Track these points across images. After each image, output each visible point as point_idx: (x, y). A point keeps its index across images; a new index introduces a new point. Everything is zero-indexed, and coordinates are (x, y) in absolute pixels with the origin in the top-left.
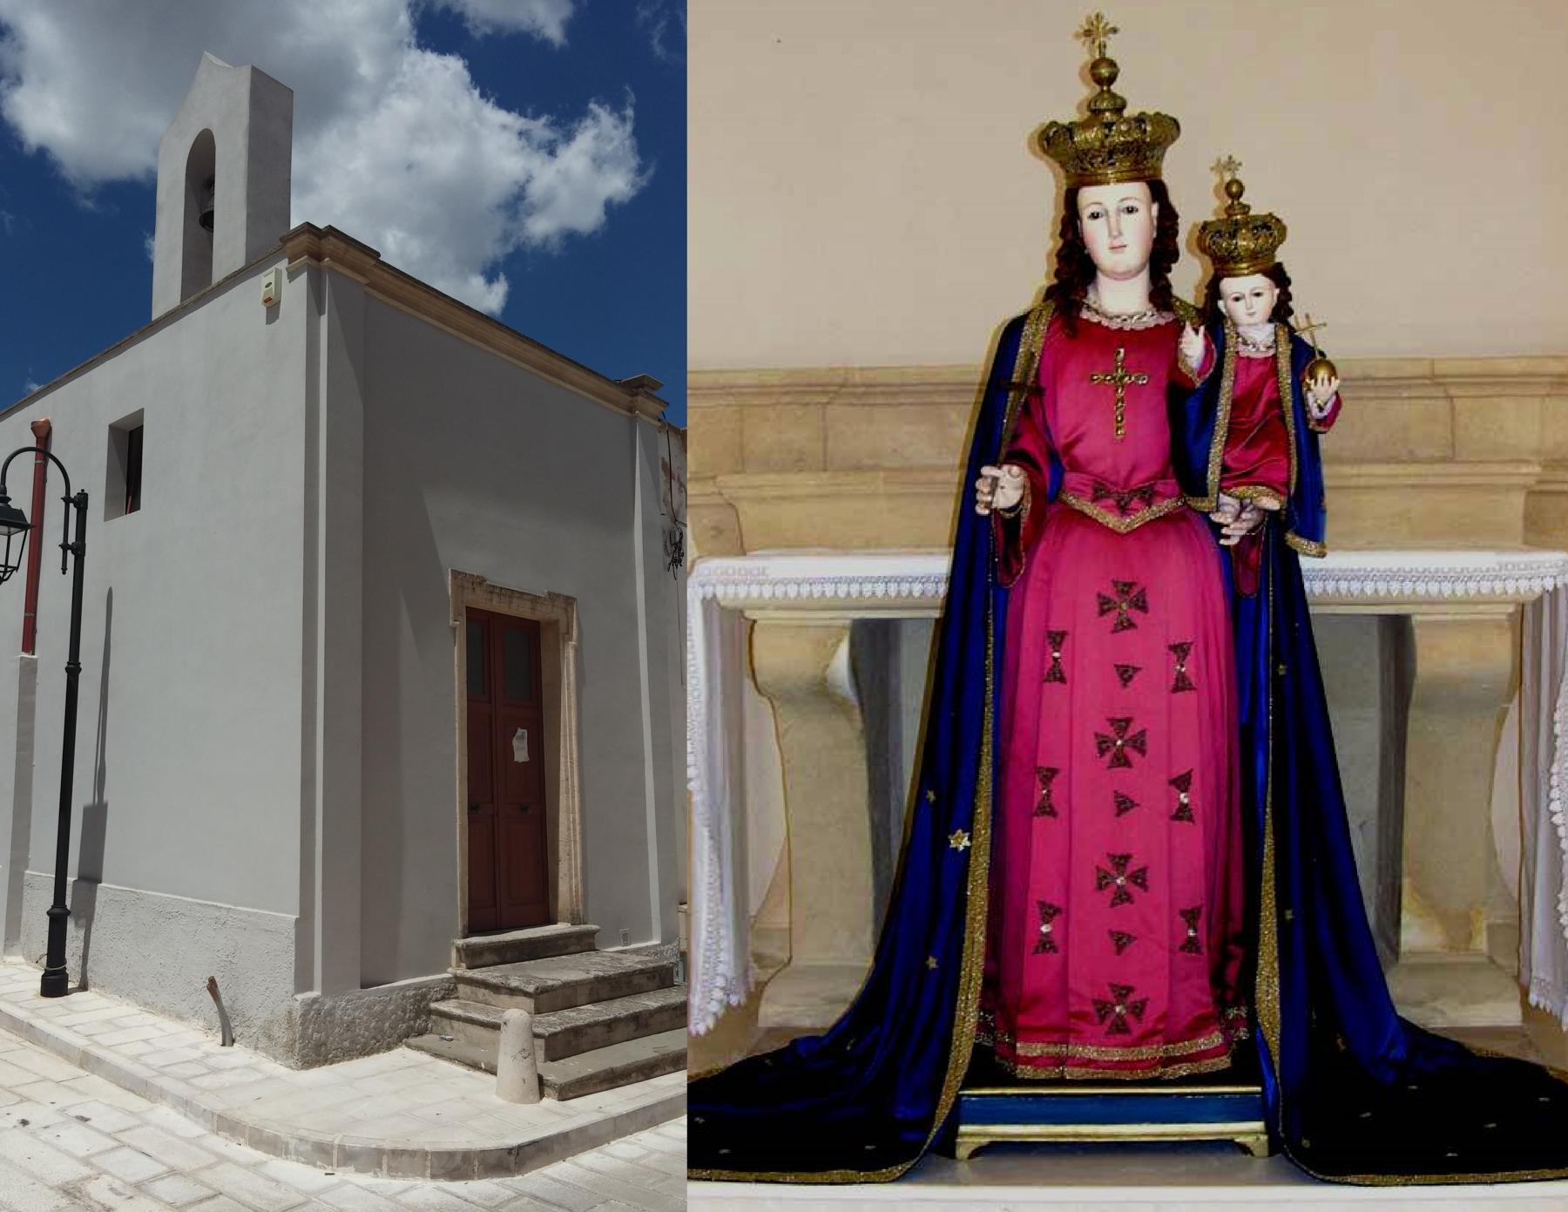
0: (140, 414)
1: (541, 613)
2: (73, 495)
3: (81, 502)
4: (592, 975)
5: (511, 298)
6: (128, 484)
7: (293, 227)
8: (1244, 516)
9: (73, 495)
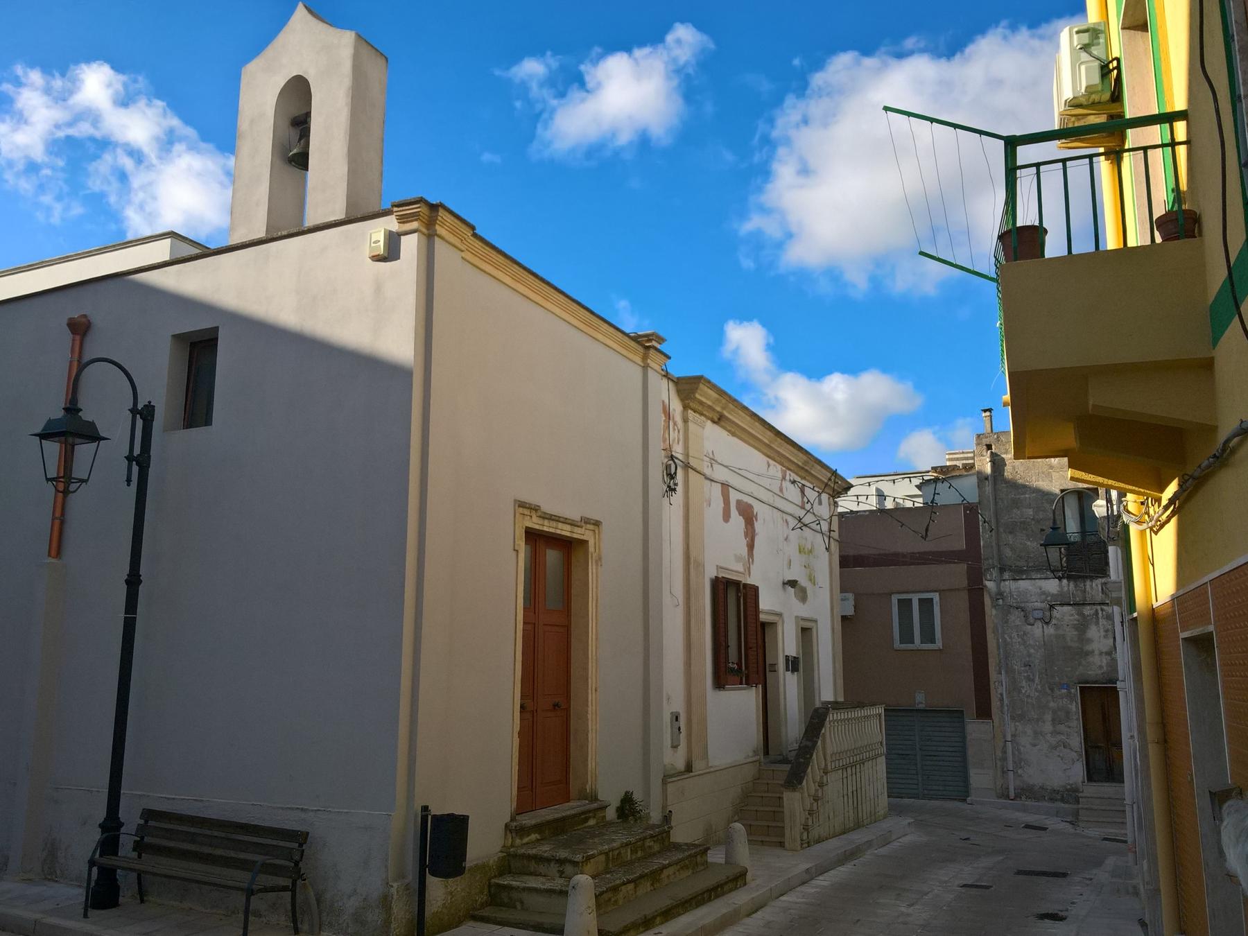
0: (216, 329)
1: (578, 533)
2: (140, 407)
3: (147, 414)
4: (827, 723)
5: (744, 317)
6: (197, 405)
7: (301, 6)
8: (1115, 63)
9: (140, 407)
